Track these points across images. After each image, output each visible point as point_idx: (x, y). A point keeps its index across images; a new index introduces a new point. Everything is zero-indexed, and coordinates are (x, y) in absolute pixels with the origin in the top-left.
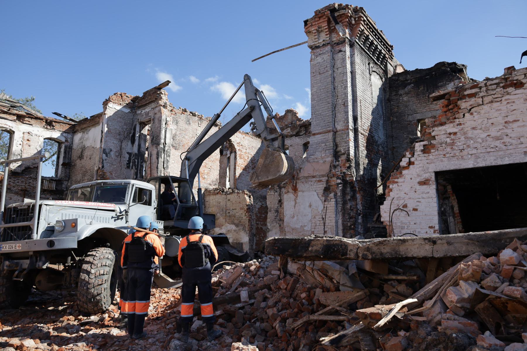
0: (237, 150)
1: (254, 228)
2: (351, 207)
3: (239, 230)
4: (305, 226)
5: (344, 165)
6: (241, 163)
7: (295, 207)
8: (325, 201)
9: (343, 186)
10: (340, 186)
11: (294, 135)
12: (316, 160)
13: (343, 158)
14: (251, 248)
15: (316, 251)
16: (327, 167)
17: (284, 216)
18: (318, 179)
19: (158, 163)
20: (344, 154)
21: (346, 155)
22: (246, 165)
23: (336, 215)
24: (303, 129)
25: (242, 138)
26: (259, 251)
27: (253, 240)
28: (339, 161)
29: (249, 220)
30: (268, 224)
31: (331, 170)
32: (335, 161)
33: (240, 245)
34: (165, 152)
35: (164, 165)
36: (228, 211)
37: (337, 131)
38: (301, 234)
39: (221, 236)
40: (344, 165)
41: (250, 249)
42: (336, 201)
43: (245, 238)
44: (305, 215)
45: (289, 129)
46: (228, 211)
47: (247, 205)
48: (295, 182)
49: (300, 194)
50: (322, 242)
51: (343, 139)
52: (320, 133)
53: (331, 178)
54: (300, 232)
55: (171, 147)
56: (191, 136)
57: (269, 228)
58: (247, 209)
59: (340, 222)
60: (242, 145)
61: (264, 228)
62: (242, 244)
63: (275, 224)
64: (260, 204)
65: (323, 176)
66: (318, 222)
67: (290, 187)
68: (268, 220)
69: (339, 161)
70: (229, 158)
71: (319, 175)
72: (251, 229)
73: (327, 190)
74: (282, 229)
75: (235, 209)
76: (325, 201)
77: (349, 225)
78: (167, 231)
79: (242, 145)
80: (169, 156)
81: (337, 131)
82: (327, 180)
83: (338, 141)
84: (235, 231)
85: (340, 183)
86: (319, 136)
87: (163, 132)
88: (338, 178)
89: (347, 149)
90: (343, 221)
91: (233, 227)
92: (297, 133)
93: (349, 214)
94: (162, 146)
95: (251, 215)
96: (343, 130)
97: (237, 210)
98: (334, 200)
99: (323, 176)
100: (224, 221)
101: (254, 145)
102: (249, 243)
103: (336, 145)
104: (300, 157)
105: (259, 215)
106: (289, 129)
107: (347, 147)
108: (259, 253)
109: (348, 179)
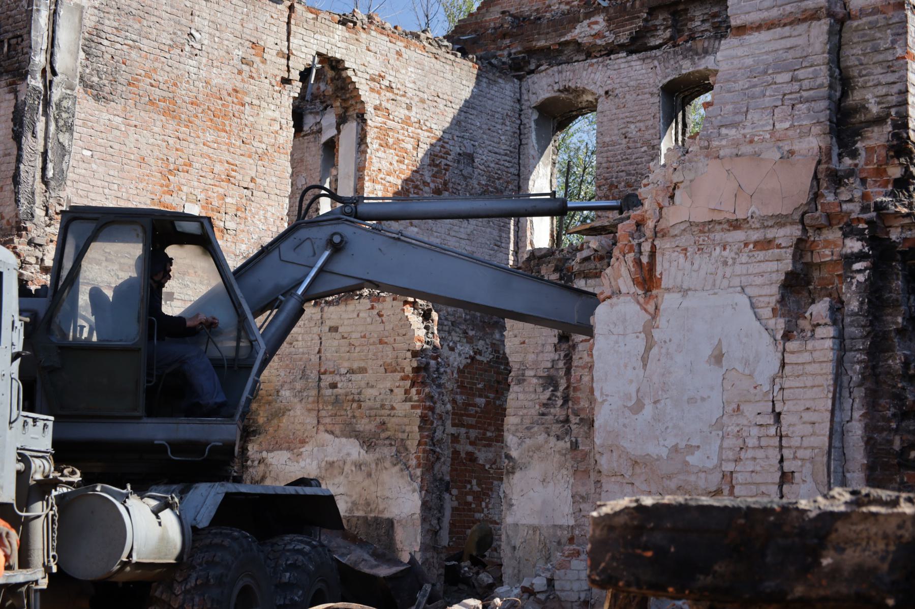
0: (369, 108)
1: (446, 453)
2: (906, 364)
3: (378, 462)
4: (691, 449)
5: (880, 171)
6: (385, 165)
7: (645, 360)
8: (787, 336)
9: (874, 268)
10: (857, 266)
11: (621, 47)
12: (746, 149)
13: (878, 137)
14: (431, 542)
15: (861, 572)
16: (796, 183)
17: (592, 401)
18: (755, 236)
19: (19, 159)
20: (879, 121)
21: (888, 128)
22: (407, 174)
23: (836, 399)
24: (660, 19)
25: (392, 56)
26: (459, 558)
27: (441, 509)
28: (854, 154)
29: (423, 418)
30: (511, 439)
31: (816, 196)
32: (835, 151)
33: (382, 530)
34: (53, 111)
35: (44, 169)
36: (327, 379)
37: (849, 16)
38: (673, 484)
39: (308, 491)
40: (880, 171)
41: (424, 548)
42: (840, 338)
43: (401, 499)
44: (691, 400)
45: (600, 18)
46: (327, 379)
47: (415, 354)
48: (646, 247)
49: (669, 301)
50: (891, 527)
51: (876, 50)
52: (770, 25)
53: (819, 229)
54: (669, 477)
55: (79, 88)
56: (165, 39)
57: (514, 454)
58: (416, 370)
59: (856, 430)
60: (390, 88)
61: (483, 456)
62: (390, 523)
63: (541, 438)
64: (468, 349)
65: (780, 221)
66: (755, 431)
67: (624, 271)
68: (511, 421)
69: (854, 154)
70: (331, 147)
71: (763, 219)
72: (429, 463)
73: (797, 286)
74: (581, 462)
75: (363, 370)
76: (787, 336)
77: (897, 445)
78: (69, 463)
79: (390, 88)
80: (70, 128)
81: (849, 16)
82: (800, 240)
83: (852, 61)
84: (359, 466)
85: (860, 256)
86: (764, 35)
87: (42, 19)
88: (849, 231)
89: (894, 99)
90: (871, 429)
91: (353, 450)
92: (633, 40)
93: (899, 397)
94: (36, 82)
95: (430, 397)
96: (875, 11)
97: (369, 376)
98: (831, 331)
99: (780, 221)
100: (311, 420)
101: (445, 88)
102: (424, 520)
103: (843, 80)
104: (647, 143)
105: (459, 398)
106: (600, 18)
107: (895, 89)
108: (466, 565)
109: (894, 235)
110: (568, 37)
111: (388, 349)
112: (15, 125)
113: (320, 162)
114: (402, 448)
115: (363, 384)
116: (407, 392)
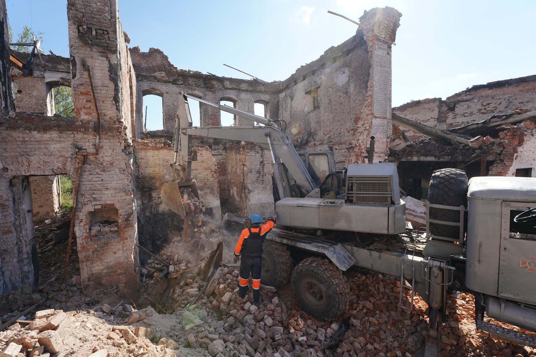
57: (250, 189)
65: (382, 153)
86: (379, 119)
99: (382, 153)
110: (153, 75)
111: (205, 164)
112: (111, 74)
113: (45, 88)
114: (212, 189)
115: (197, 173)
116: (213, 175)
